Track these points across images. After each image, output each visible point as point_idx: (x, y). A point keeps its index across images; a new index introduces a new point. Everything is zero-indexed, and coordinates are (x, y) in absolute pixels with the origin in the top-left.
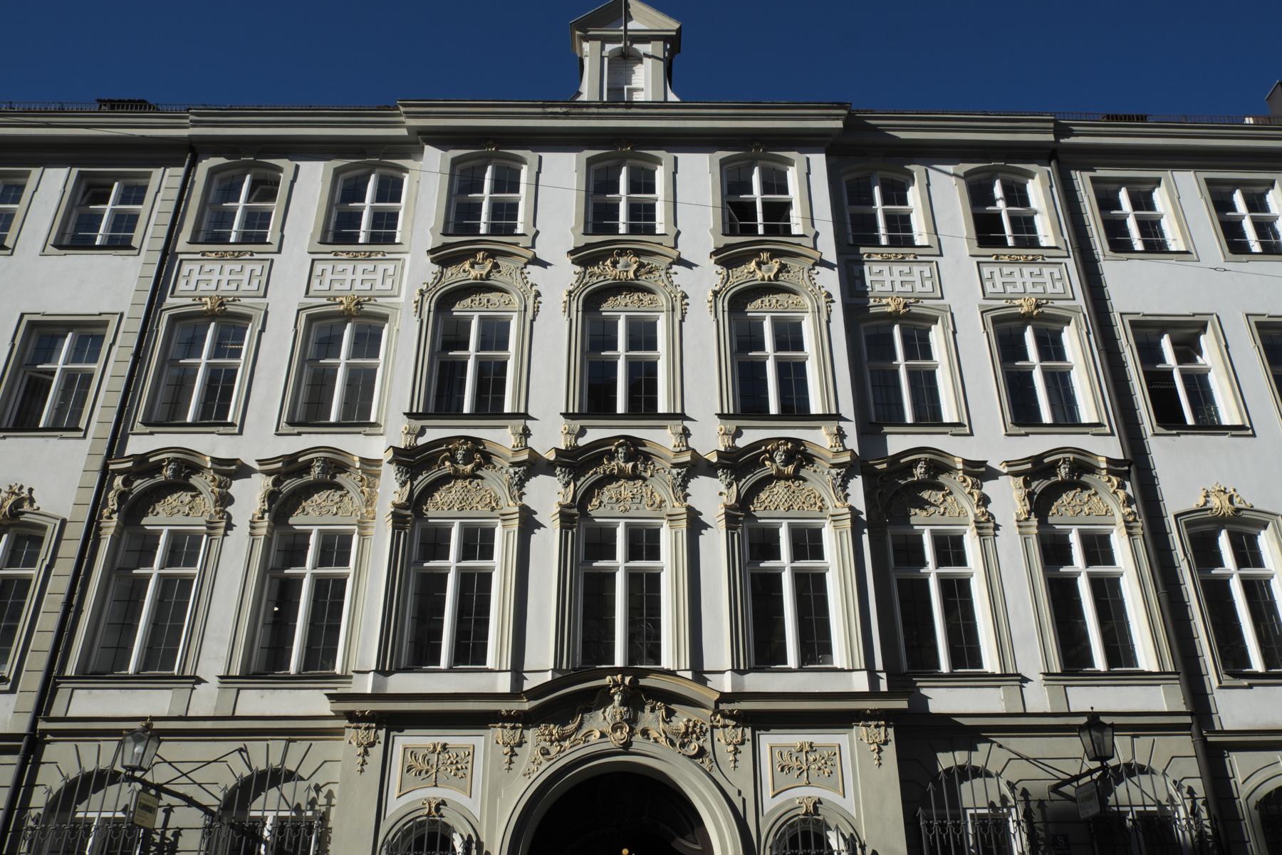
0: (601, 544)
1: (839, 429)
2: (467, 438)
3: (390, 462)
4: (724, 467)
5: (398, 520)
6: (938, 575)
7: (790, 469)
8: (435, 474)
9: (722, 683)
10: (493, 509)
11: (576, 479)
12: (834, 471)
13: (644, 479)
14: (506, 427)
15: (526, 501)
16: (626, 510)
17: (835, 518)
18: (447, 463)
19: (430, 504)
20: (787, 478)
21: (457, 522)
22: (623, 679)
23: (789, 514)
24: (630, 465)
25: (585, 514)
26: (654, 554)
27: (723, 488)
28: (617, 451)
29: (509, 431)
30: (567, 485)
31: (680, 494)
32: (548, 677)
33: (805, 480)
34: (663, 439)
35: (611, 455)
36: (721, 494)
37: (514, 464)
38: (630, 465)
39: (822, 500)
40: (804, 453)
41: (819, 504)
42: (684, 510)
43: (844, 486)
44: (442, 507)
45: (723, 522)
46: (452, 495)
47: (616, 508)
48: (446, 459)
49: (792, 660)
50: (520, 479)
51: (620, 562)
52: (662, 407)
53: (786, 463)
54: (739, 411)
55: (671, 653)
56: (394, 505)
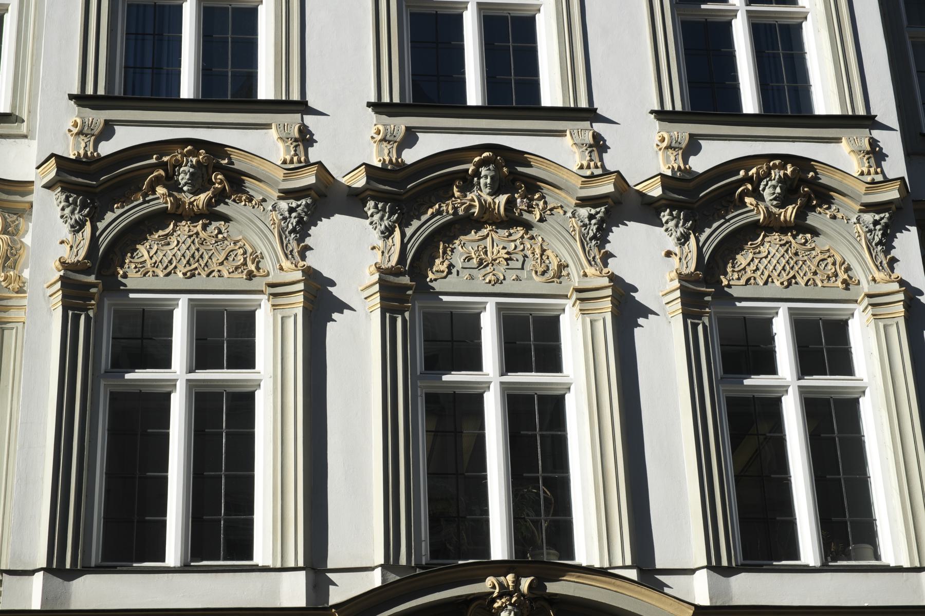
0: (145, 339)
1: (873, 143)
2: (198, 144)
3: (49, 186)
4: (672, 205)
5: (74, 292)
6: (802, 390)
7: (790, 212)
8: (137, 209)
9: (690, 591)
10: (251, 276)
11: (404, 223)
12: (869, 218)
13: (528, 226)
14: (267, 126)
15: (312, 260)
16: (497, 281)
17: (584, 295)
18: (160, 190)
19: (130, 266)
20: (784, 229)
21: (183, 300)
22: (517, 583)
23: (498, 289)
24: (502, 199)
25: (424, 289)
26: (244, 357)
27: (671, 243)
28: (477, 174)
29: (273, 133)
30: (387, 233)
31: (293, 245)
32: (375, 580)
33: (815, 232)
34: (262, 145)
35: (468, 182)
36: (669, 254)
37: (287, 194)
38: (502, 199)
39: (848, 269)
40: (814, 184)
41: (842, 276)
42: (299, 275)
43: (887, 244)
44: (151, 271)
45: (678, 305)
46: (170, 251)
47: (477, 277)
48: (158, 181)
49: (809, 549)
50: (300, 221)
51: (179, 371)
52: (266, 90)
53: (783, 201)
54: (409, 100)
55: (593, 538)
56: (63, 263)
